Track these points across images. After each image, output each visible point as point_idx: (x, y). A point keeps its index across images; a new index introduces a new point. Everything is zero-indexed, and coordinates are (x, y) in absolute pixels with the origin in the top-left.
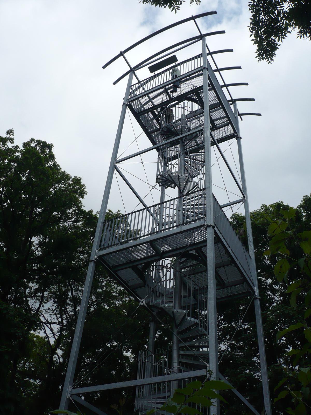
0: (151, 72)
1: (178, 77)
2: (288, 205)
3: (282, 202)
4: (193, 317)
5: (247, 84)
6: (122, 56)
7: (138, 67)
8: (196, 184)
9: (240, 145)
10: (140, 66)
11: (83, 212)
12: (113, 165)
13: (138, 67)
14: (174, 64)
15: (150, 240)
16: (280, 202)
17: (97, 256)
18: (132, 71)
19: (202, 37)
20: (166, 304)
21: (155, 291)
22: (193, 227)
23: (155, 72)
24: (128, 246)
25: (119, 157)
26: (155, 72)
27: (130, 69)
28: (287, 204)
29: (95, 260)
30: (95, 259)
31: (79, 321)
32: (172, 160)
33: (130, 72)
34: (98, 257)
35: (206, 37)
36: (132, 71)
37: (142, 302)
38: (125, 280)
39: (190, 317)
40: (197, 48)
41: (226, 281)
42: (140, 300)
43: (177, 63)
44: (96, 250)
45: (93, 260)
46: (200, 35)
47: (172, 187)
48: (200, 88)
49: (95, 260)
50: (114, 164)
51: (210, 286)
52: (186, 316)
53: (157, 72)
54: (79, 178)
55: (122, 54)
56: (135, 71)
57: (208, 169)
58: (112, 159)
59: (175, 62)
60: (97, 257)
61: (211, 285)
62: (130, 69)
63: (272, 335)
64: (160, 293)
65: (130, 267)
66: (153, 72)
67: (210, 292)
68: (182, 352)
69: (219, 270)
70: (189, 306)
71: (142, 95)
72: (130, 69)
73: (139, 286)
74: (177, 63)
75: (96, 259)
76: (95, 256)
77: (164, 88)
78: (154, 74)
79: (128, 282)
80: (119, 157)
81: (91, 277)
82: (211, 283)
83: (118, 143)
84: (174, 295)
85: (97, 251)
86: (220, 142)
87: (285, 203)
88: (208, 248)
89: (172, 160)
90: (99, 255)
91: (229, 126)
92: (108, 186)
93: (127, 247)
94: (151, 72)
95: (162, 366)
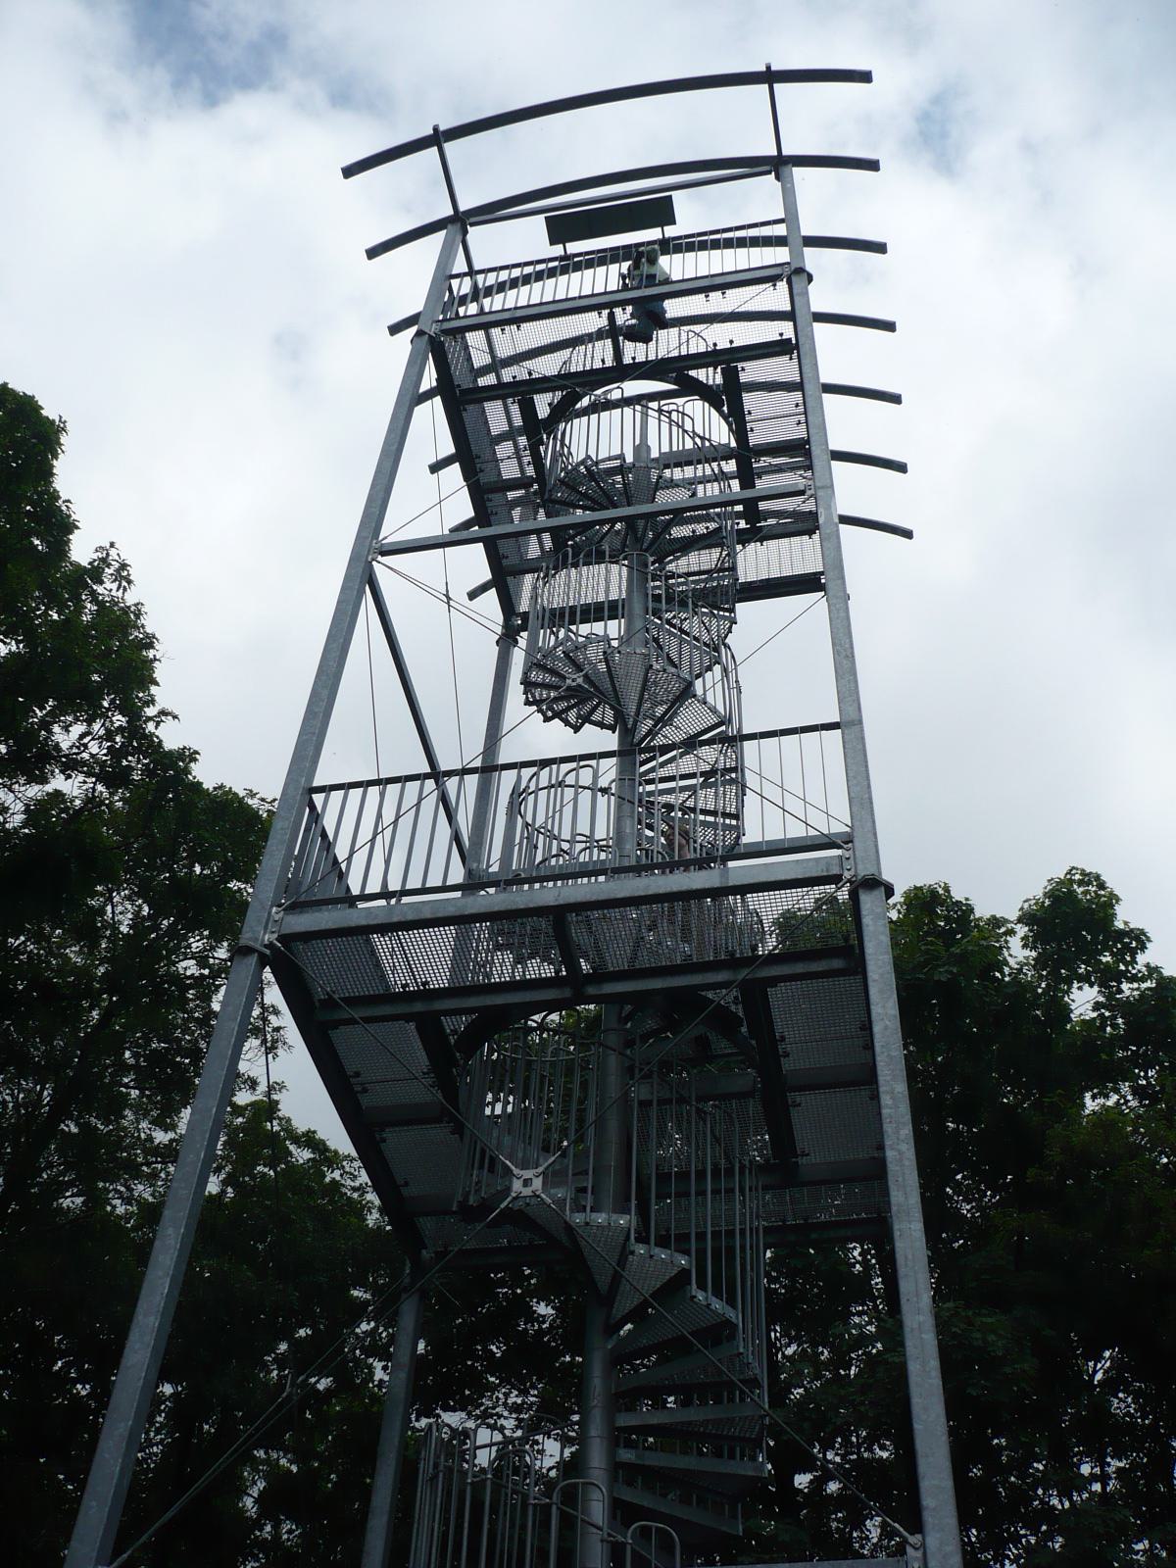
0: (553, 242)
1: (661, 283)
2: (970, 905)
3: (947, 889)
4: (717, 1294)
5: (895, 399)
6: (436, 148)
7: (491, 212)
8: (714, 720)
9: (498, 727)
10: (499, 211)
11: (151, 747)
12: (367, 557)
13: (491, 212)
14: (653, 234)
15: (562, 902)
16: (940, 886)
17: (276, 936)
18: (458, 221)
19: (778, 165)
20: (594, 1215)
21: (483, 1152)
22: (783, 878)
23: (567, 245)
24: (446, 914)
25: (393, 529)
26: (567, 245)
27: (451, 212)
28: (967, 899)
29: (268, 952)
30: (266, 946)
31: (170, 1231)
32: (578, 620)
33: (449, 226)
34: (282, 938)
35: (795, 169)
36: (460, 221)
37: (527, 1183)
38: (357, 1074)
39: (706, 1291)
40: (758, 198)
41: (808, 1155)
42: (516, 1171)
43: (671, 231)
44: (272, 907)
45: (258, 946)
46: (776, 153)
47: (567, 723)
48: (771, 346)
49: (268, 952)
50: (368, 554)
51: (899, 1151)
52: (690, 1284)
53: (574, 247)
54: (136, 605)
55: (437, 139)
56: (472, 225)
57: (845, 651)
58: (364, 534)
59: (662, 225)
60: (277, 939)
61: (904, 1147)
62: (451, 212)
63: (1162, 1427)
64: (489, 1171)
65: (407, 1018)
66: (558, 243)
67: (900, 1179)
68: (626, 1455)
69: (798, 1100)
70: (701, 1236)
71: (506, 316)
72: (452, 213)
73: (412, 1117)
74: (671, 231)
75: (270, 946)
76: (265, 934)
77: (605, 312)
78: (563, 253)
79: (365, 1090)
80: (393, 529)
81: (239, 1026)
82: (902, 1137)
83: (390, 475)
84: (593, 1182)
85: (274, 909)
86: (754, 594)
87: (958, 895)
88: (874, 981)
89: (578, 620)
90: (286, 931)
91: (814, 536)
92: (342, 640)
93: (440, 915)
94: (553, 242)
95: (580, 1516)
